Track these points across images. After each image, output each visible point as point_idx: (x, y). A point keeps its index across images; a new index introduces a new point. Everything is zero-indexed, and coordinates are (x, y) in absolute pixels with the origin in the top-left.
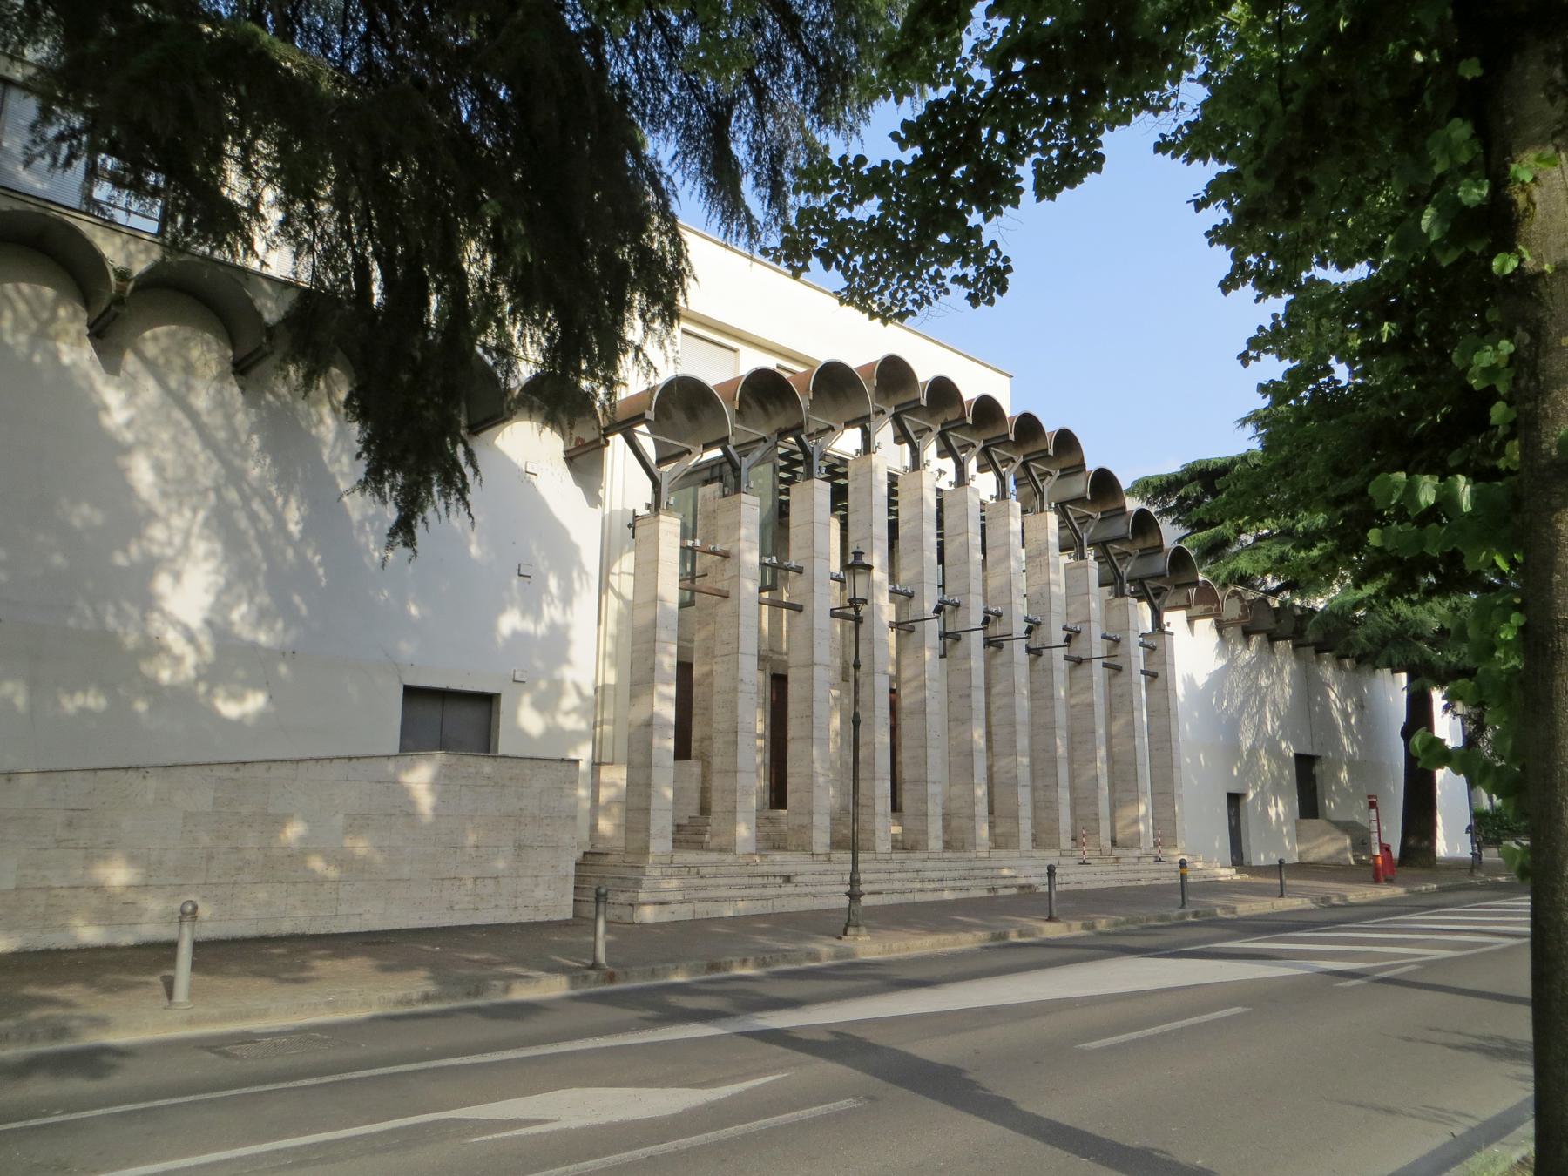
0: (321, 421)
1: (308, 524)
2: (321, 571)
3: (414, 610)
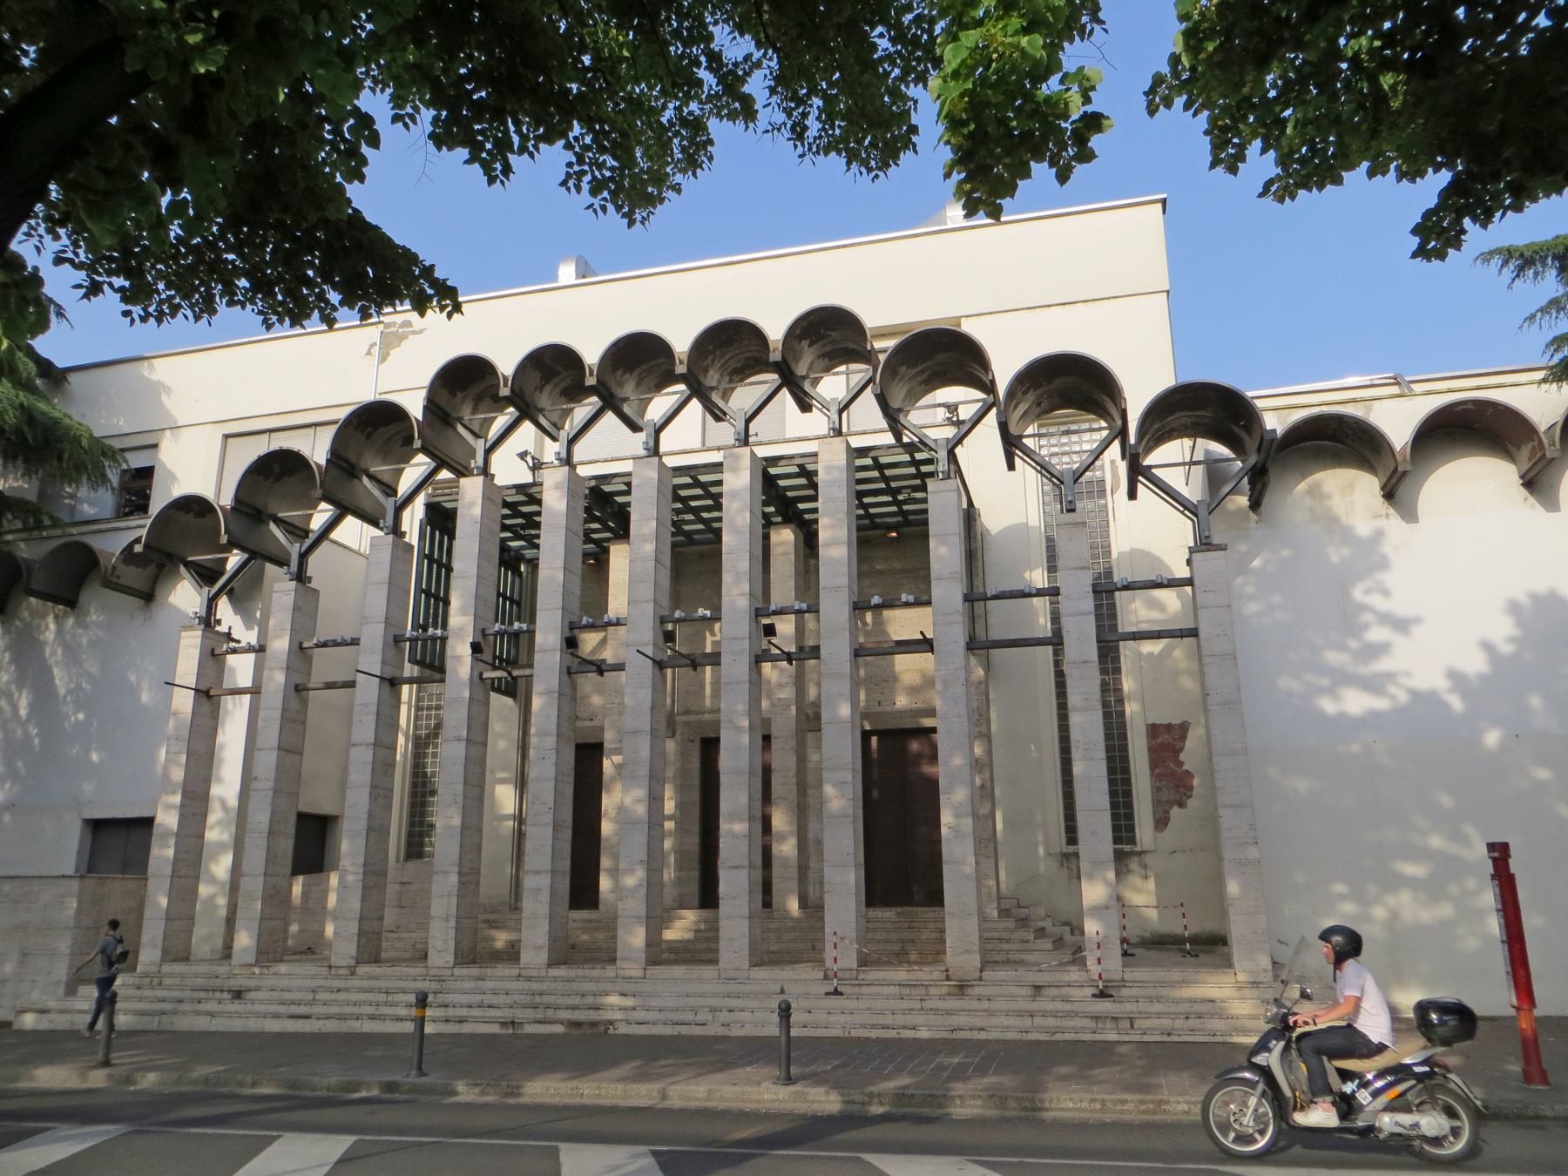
0: (47, 628)
1: (32, 707)
2: (36, 741)
3: (95, 757)
